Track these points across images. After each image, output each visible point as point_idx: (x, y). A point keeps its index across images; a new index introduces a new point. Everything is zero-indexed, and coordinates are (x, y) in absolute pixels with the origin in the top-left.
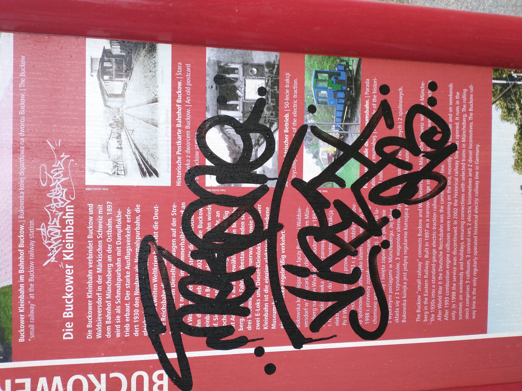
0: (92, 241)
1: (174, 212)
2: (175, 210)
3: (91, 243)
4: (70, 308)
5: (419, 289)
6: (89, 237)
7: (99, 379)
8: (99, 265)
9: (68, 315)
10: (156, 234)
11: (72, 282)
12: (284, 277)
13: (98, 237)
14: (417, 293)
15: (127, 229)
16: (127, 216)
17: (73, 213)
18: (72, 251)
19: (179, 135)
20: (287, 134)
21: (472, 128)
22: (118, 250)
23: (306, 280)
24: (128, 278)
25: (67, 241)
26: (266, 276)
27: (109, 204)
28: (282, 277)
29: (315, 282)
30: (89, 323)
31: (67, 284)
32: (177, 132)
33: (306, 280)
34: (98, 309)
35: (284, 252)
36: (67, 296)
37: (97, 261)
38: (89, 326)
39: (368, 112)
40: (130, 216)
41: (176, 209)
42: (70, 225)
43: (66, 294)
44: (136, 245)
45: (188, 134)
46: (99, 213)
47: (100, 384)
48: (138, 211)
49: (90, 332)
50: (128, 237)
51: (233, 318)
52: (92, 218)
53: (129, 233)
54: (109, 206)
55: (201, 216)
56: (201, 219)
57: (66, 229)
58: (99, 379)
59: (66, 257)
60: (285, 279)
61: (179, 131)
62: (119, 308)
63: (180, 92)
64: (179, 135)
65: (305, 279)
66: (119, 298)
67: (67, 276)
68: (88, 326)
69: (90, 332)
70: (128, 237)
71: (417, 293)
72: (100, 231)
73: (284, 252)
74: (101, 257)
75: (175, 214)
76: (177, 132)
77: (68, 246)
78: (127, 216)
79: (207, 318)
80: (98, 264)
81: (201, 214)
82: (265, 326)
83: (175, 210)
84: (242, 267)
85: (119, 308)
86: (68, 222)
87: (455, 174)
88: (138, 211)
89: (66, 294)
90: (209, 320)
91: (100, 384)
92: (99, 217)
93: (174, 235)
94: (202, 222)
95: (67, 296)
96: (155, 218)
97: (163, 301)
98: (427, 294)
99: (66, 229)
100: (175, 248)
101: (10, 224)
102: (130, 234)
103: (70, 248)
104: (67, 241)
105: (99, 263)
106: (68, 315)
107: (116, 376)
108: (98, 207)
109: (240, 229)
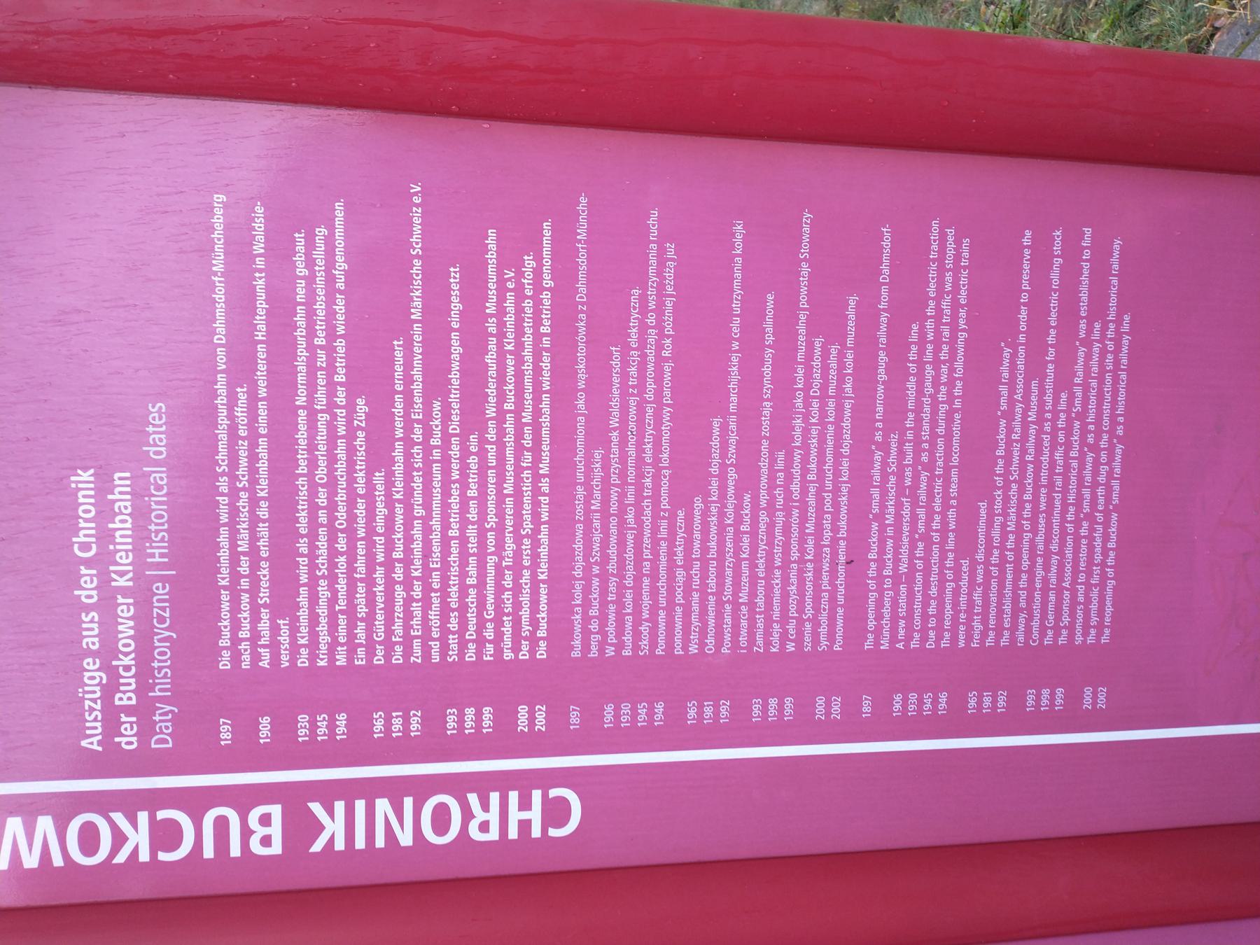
1: (804, 253)
3: (509, 621)
5: (1003, 406)
6: (222, 643)
15: (378, 575)
16: (526, 281)
21: (383, 606)
24: (417, 297)
27: (573, 710)
32: (1047, 368)
34: (524, 557)
39: (326, 628)
40: (531, 282)
44: (262, 632)
50: (380, 592)
51: (266, 662)
52: (248, 596)
53: (380, 583)
54: (575, 713)
56: (1076, 441)
62: (305, 543)
65: (628, 488)
68: (121, 699)
70: (380, 592)
76: (1047, 368)
78: (526, 281)
84: (524, 613)
87: (356, 612)
90: (547, 553)
93: (300, 247)
96: (377, 660)
98: (437, 563)
100: (401, 596)
102: (383, 586)
104: (434, 580)
108: (318, 440)
109: (367, 610)
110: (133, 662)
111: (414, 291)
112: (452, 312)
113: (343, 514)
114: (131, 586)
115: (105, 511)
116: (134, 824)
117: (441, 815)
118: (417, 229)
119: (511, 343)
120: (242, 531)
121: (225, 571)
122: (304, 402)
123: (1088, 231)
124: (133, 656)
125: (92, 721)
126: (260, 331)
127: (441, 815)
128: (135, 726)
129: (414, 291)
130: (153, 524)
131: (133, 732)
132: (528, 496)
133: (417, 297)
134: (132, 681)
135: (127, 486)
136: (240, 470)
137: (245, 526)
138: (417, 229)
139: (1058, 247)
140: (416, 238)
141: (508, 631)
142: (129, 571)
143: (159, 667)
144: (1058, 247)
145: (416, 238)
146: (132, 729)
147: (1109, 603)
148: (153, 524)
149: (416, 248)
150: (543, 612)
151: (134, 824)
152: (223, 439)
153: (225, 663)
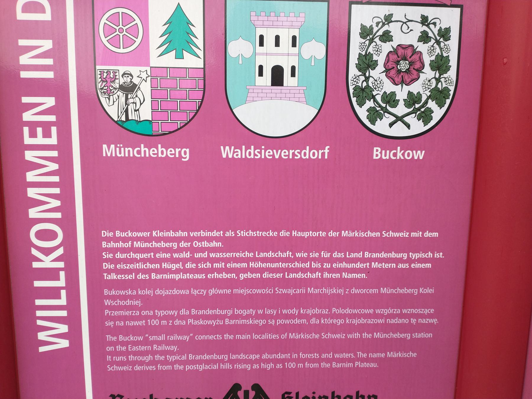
0: (222, 235)
1: (241, 234)
2: (259, 234)
3: (220, 235)
8: (351, 233)
9: (118, 234)
10: (310, 234)
12: (175, 267)
13: (384, 233)
14: (147, 335)
19: (319, 234)
20: (340, 234)
22: (418, 233)
23: (302, 291)
24: (354, 234)
26: (328, 267)
28: (175, 265)
29: (111, 304)
30: (121, 233)
33: (302, 291)
35: (192, 235)
36: (271, 232)
37: (356, 231)
38: (118, 234)
41: (260, 235)
42: (175, 234)
45: (434, 234)
46: (412, 233)
48: (282, 234)
49: (111, 234)
55: (132, 234)
56: (127, 234)
59: (48, 203)
60: (259, 324)
61: (323, 234)
62: (232, 234)
63: (130, 234)
64: (319, 234)
66: (389, 235)
69: (111, 234)
71: (147, 335)
72: (392, 234)
73: (192, 235)
74: (360, 236)
75: (239, 234)
79: (171, 233)
80: (352, 232)
81: (135, 234)
82: (157, 233)
83: (259, 234)
85: (232, 234)
88: (282, 234)
92: (408, 233)
94: (124, 236)
95: (271, 232)
97: (174, 233)
105: (353, 233)
110: (131, 340)
111: (358, 233)
112: (210, 233)
113: (427, 235)
114: (400, 148)
115: (210, 239)
116: (140, 293)
117: (48, 235)
118: (397, 235)
119: (157, 235)
120: (353, 233)
121: (161, 234)
122: (141, 234)
123: (436, 234)
124: (402, 158)
125: (361, 234)
126: (297, 233)
127: (48, 235)
128: (173, 156)
129: (358, 233)
130: (322, 232)
131: (114, 340)
132: (254, 234)
133: (354, 234)
134: (387, 157)
135: (325, 277)
136: (392, 233)
137: (356, 235)
138: (397, 235)
139: (312, 234)
140: (392, 234)
141: (214, 234)
142: (304, 313)
143: (257, 233)
144: (312, 234)
145: (392, 234)
146: (431, 292)
147: (166, 234)
148: (322, 232)
149: (386, 234)
150: (132, 234)
151: (140, 293)
152: (298, 234)
153: (105, 234)
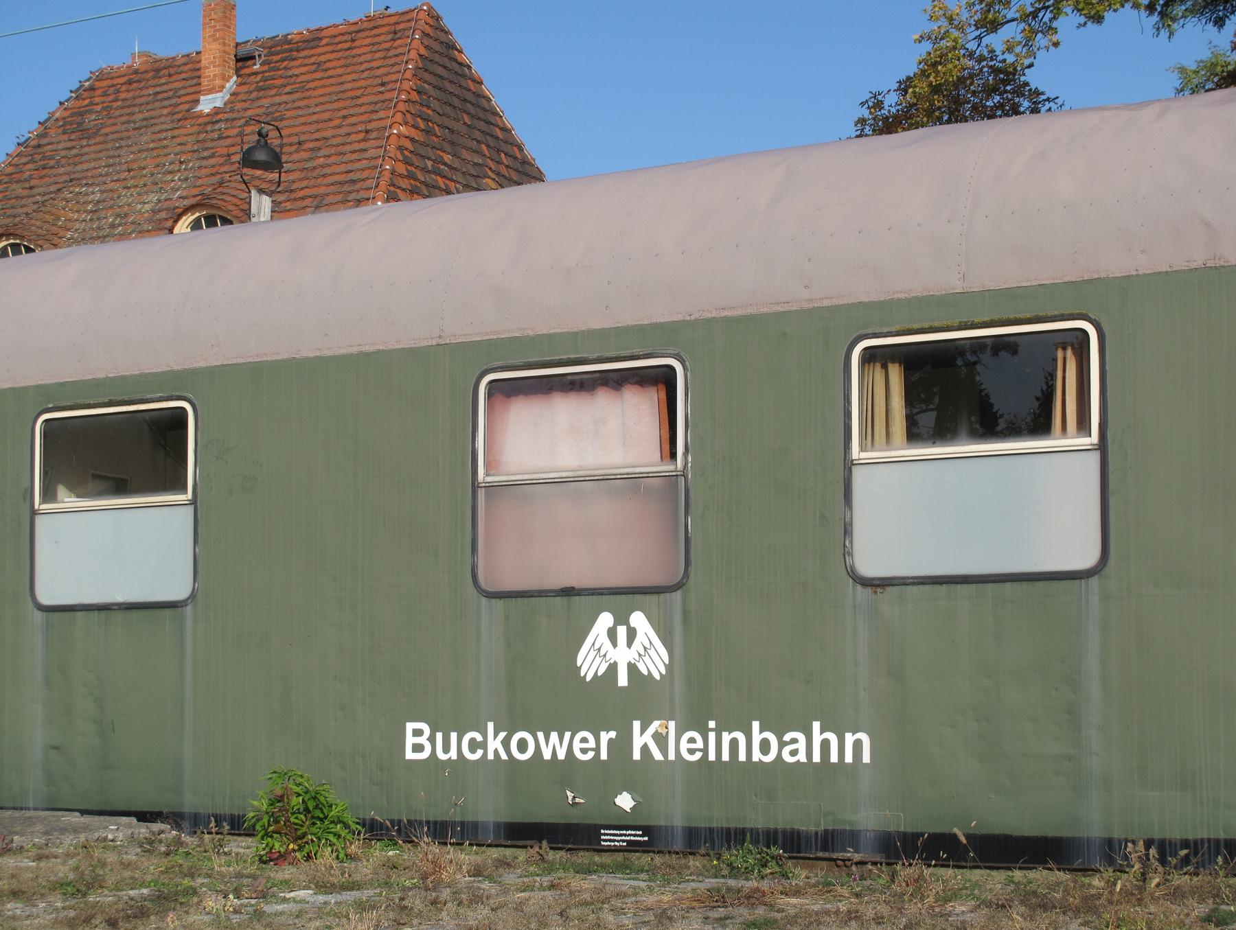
4: (446, 749)
7: (496, 752)
9: (418, 740)
11: (547, 755)
17: (834, 758)
18: (672, 756)
25: (712, 736)
31: (540, 735)
36: (495, 736)
43: (502, 735)
47: (494, 739)
57: (761, 731)
58: (496, 752)
67: (568, 735)
77: (692, 740)
86: (794, 741)
89: (502, 735)
91: (494, 739)
95: (495, 736)
99: (761, 731)
101: (147, 826)
103: (684, 746)
104: (712, 736)
106: (418, 740)
107: (670, 363)
